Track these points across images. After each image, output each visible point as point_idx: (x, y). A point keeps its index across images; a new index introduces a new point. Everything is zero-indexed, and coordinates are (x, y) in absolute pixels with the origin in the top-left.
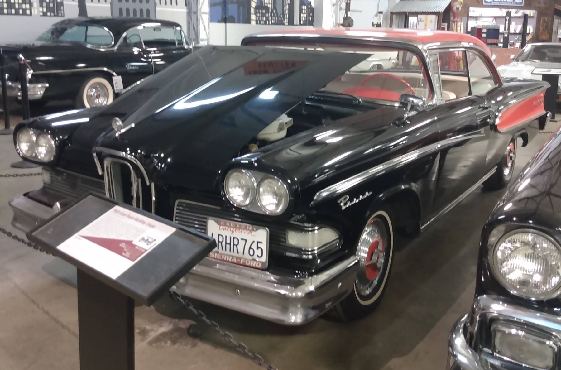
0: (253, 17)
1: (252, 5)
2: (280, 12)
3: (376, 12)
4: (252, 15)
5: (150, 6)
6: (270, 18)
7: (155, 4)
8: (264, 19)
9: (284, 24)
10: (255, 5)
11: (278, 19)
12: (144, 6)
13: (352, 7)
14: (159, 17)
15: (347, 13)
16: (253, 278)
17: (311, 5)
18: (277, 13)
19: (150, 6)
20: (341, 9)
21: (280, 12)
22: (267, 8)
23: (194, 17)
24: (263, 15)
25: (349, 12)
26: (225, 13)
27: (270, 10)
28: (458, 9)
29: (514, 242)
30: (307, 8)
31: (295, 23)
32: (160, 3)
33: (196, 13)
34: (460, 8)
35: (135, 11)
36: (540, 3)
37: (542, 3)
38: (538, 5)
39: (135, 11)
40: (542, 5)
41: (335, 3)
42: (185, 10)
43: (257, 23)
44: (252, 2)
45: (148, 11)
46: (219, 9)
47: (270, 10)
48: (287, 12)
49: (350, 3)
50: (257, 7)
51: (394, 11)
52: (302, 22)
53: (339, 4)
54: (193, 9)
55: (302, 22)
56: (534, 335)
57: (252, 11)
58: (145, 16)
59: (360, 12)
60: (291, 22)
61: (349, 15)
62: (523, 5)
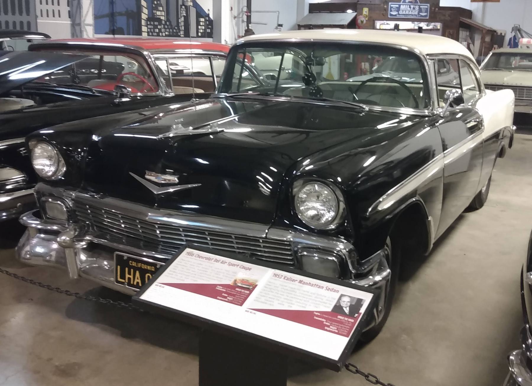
0: (144, 29)
1: (143, 17)
2: (174, 24)
3: (276, 25)
4: (143, 27)
5: (30, 18)
6: (163, 30)
7: (36, 17)
8: (157, 30)
9: (179, 36)
10: (147, 16)
11: (173, 31)
12: (25, 18)
13: (253, 20)
14: (40, 31)
15: (248, 26)
16: (300, 300)
17: (209, 17)
18: (171, 25)
19: (30, 18)
20: (243, 21)
21: (174, 24)
22: (159, 20)
23: (77, 28)
24: (155, 27)
25: (250, 25)
26: (113, 25)
27: (163, 22)
28: (362, 22)
29: (318, 197)
30: (206, 20)
31: (191, 35)
32: (42, 16)
33: (79, 24)
34: (365, 22)
35: (14, 23)
36: (445, 15)
37: (447, 16)
38: (443, 18)
39: (14, 23)
40: (448, 18)
41: (236, 15)
42: (69, 22)
43: (148, 35)
44: (143, 14)
45: (29, 23)
46: (107, 20)
47: (163, 22)
48: (182, 24)
49: (250, 16)
50: (148, 20)
51: (301, 24)
52: (200, 34)
53: (241, 16)
54: (77, 21)
55: (200, 34)
56: (217, 232)
57: (143, 22)
58: (25, 29)
59: (266, 24)
60: (187, 35)
61: (250, 28)
62: (428, 18)
